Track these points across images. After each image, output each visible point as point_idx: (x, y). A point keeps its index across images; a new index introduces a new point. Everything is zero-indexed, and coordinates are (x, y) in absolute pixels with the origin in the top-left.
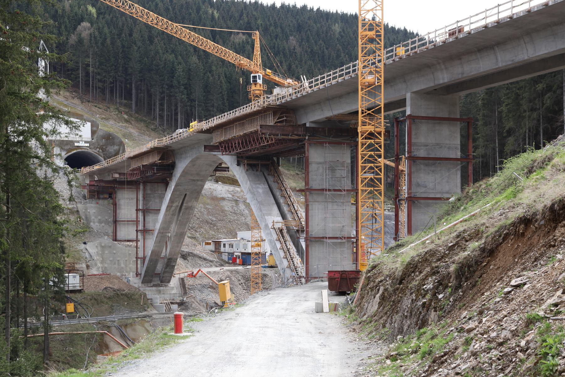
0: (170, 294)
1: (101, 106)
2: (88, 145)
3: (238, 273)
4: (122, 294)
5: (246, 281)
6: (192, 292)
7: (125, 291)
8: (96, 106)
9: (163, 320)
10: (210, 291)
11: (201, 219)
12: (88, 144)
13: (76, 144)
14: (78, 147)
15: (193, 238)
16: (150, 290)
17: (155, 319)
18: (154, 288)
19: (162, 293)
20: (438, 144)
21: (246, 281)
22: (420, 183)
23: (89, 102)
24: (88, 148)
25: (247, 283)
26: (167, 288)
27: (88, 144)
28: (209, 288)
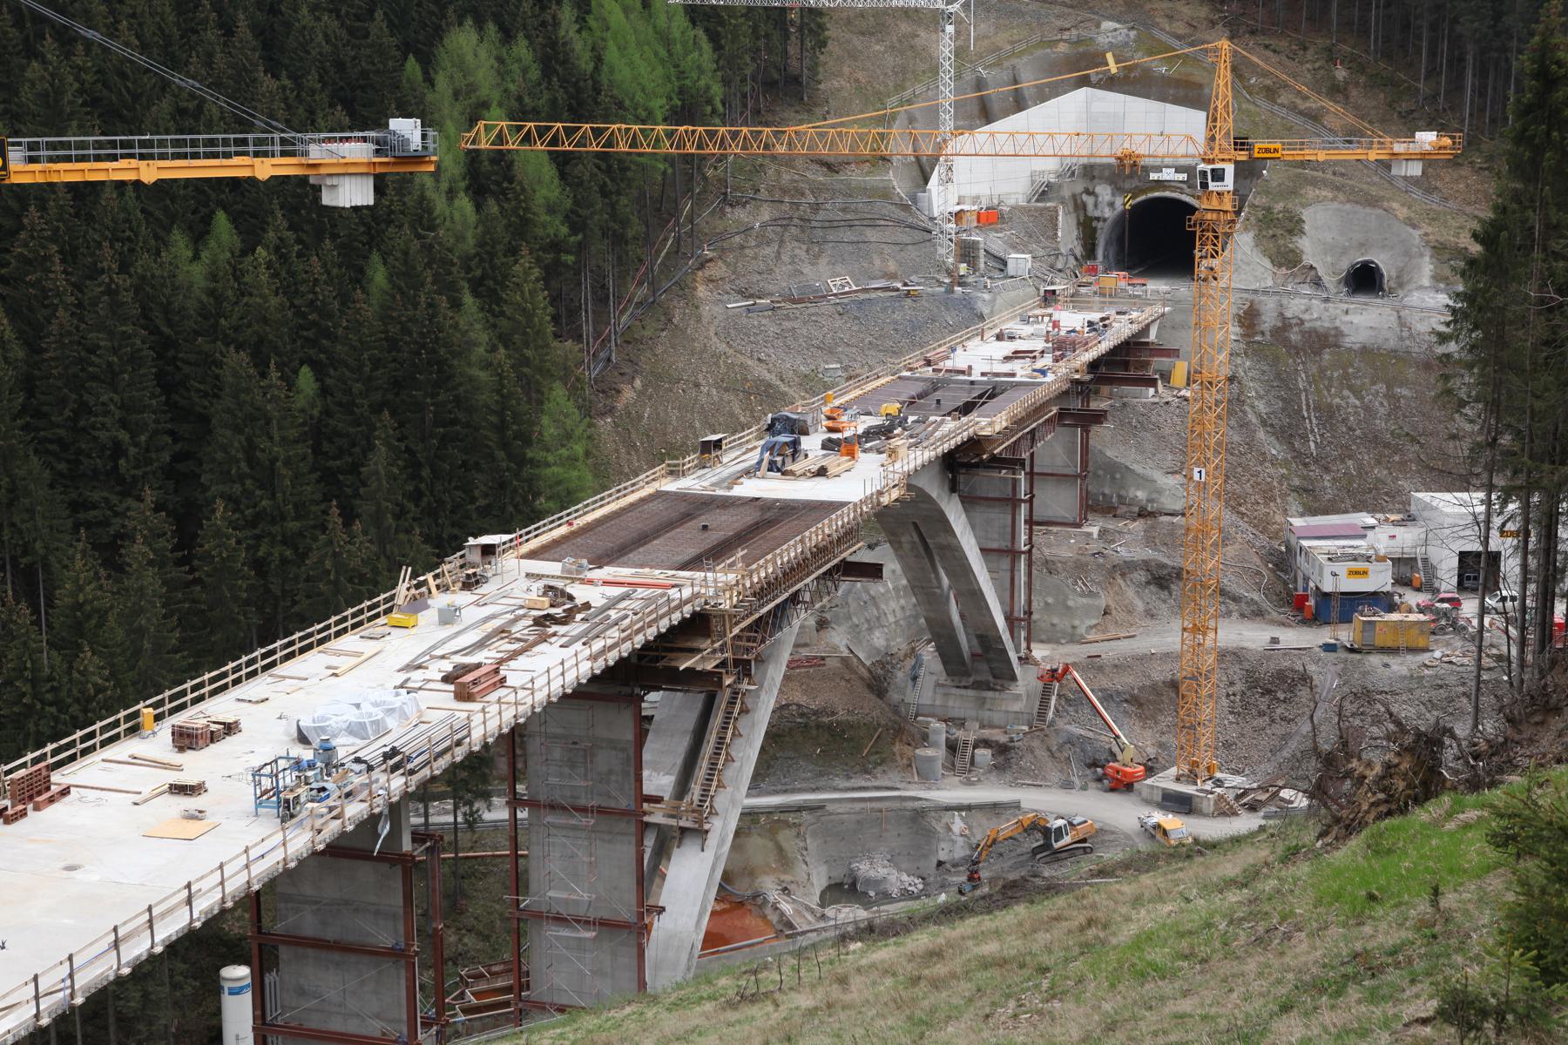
0: (1007, 712)
1: (1284, 44)
2: (1183, 177)
3: (1240, 662)
4: (819, 726)
5: (1249, 688)
6: (1071, 709)
7: (833, 714)
8: (1267, 47)
9: (859, 817)
10: (1125, 712)
11: (1358, 432)
12: (1185, 175)
13: (1153, 176)
14: (1160, 184)
15: (1306, 490)
16: (962, 696)
17: (830, 814)
18: (970, 693)
19: (987, 706)
20: (347, 903)
21: (1249, 688)
22: (306, 988)
23: (1253, 33)
24: (1184, 186)
25: (1249, 693)
26: (1003, 695)
27: (1185, 175)
28: (1126, 701)
